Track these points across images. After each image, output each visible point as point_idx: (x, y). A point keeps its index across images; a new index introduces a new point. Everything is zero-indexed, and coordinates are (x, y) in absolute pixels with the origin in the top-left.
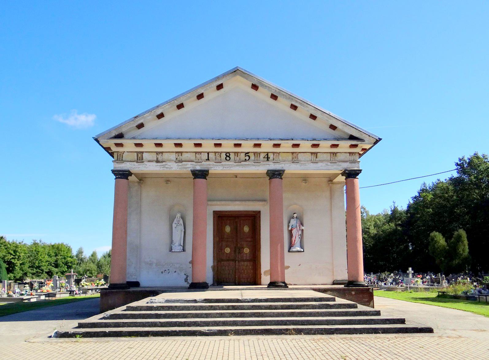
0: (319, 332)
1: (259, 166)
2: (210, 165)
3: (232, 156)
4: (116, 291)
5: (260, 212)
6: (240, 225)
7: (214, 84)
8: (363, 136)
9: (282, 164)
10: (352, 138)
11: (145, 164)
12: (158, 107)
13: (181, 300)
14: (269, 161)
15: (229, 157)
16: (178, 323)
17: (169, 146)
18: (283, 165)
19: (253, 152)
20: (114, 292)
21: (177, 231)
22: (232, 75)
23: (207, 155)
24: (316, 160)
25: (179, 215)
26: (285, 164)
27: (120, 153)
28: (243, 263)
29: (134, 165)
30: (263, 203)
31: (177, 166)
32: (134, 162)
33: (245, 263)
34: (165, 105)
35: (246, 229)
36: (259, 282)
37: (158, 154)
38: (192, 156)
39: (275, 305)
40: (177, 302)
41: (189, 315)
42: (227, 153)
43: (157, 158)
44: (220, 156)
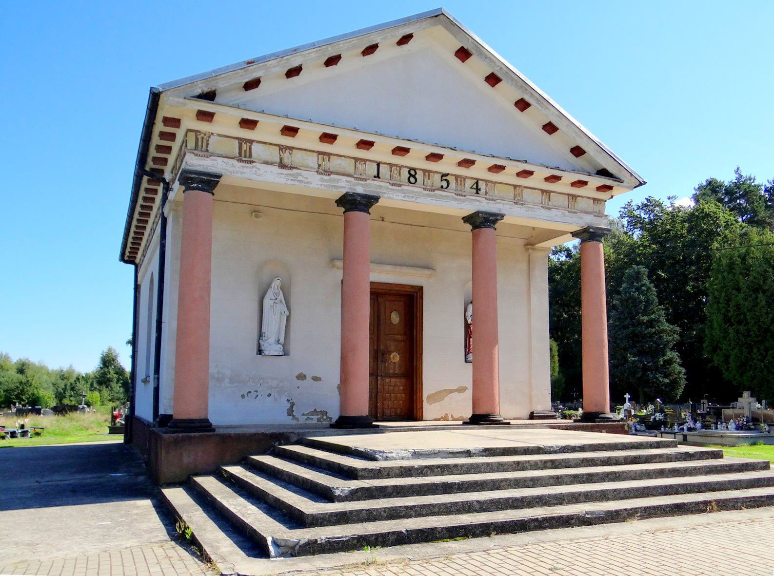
0: (748, 503)
1: (464, 201)
2: (380, 187)
3: (420, 176)
4: (201, 435)
5: (421, 289)
6: (385, 308)
7: (400, 32)
8: (622, 173)
9: (500, 203)
10: (603, 173)
11: (255, 167)
12: (295, 50)
13: (444, 452)
14: (478, 195)
15: (414, 177)
16: (511, 501)
17: (308, 137)
18: (501, 206)
19: (455, 175)
20: (194, 437)
21: (274, 315)
22: (429, 20)
23: (376, 166)
24: (548, 205)
25: (276, 283)
26: (504, 204)
27: (202, 135)
28: (388, 380)
29: (233, 166)
30: (427, 272)
31: (320, 180)
32: (232, 158)
33: (393, 380)
34: (310, 51)
35: (395, 318)
36: (419, 416)
37: (284, 150)
38: (348, 166)
39: (616, 457)
40: (436, 455)
41: (502, 484)
42: (411, 169)
43: (281, 159)
44: (400, 174)
